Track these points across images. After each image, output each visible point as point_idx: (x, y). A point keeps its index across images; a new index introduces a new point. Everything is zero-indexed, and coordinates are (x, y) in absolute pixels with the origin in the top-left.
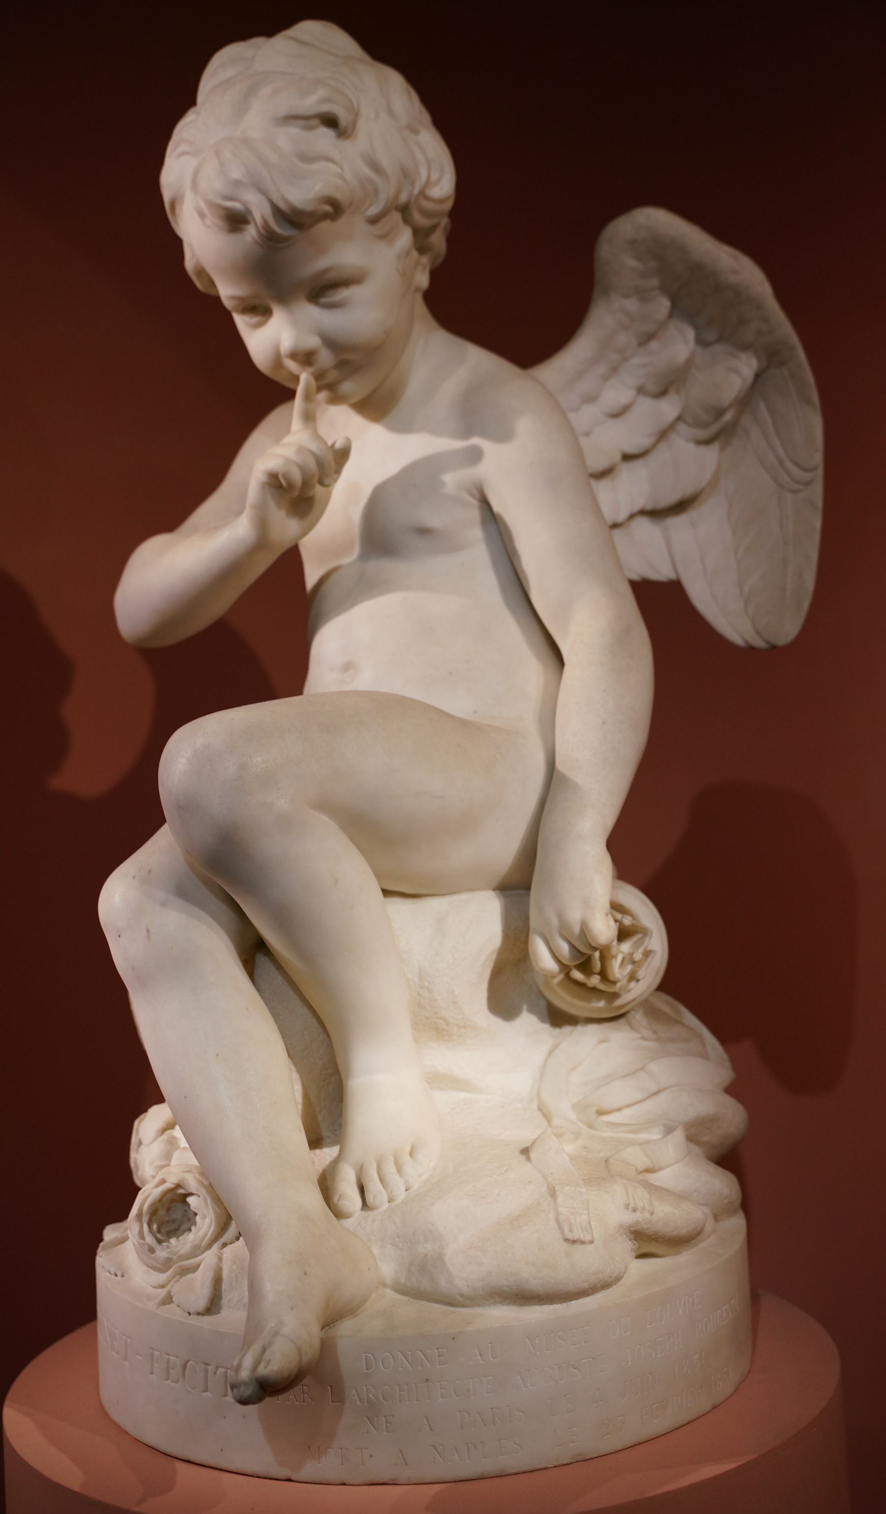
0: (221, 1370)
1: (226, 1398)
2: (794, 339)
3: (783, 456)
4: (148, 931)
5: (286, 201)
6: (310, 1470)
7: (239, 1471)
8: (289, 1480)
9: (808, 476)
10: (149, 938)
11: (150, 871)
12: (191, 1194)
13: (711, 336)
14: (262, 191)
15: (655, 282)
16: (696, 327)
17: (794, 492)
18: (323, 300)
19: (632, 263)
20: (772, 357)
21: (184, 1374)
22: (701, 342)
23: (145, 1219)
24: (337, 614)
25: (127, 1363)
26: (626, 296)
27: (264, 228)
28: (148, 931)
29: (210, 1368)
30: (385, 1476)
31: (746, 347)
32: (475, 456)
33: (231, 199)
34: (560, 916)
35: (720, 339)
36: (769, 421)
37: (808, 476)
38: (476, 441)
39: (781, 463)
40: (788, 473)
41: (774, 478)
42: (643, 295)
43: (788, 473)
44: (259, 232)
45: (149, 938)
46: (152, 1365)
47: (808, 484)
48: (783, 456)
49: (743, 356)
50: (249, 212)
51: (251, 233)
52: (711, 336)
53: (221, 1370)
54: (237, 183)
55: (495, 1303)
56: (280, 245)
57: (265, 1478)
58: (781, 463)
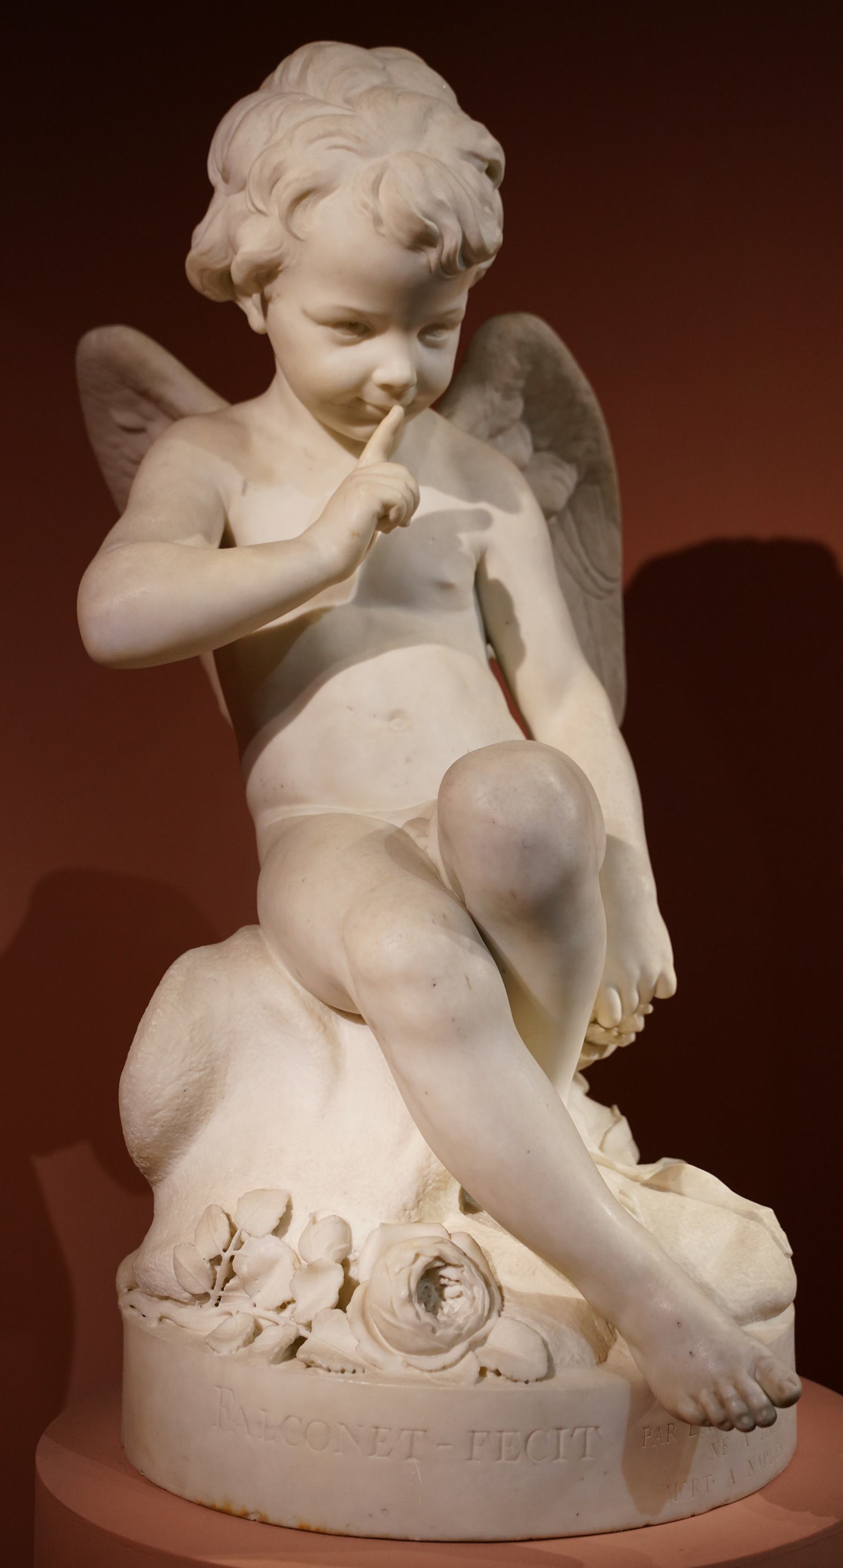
0: (578, 1432)
1: (585, 1459)
2: (612, 463)
3: (587, 563)
4: (467, 979)
5: (480, 237)
6: (669, 1509)
7: (597, 1531)
8: (647, 1526)
9: (611, 585)
10: (470, 987)
11: (444, 916)
12: (447, 1265)
13: (544, 443)
14: (460, 221)
15: (521, 383)
16: (534, 433)
17: (599, 598)
18: (429, 338)
19: (514, 361)
20: (590, 475)
21: (526, 1448)
22: (536, 449)
23: (415, 1298)
24: (363, 659)
25: (413, 1461)
26: (497, 390)
27: (448, 257)
28: (467, 979)
29: (563, 1433)
30: (721, 1500)
31: (570, 460)
32: (484, 521)
33: (430, 219)
34: (644, 970)
35: (550, 448)
36: (574, 529)
37: (611, 585)
38: (483, 506)
39: (586, 570)
40: (593, 580)
41: (580, 583)
42: (507, 393)
43: (593, 580)
44: (439, 259)
45: (470, 987)
46: (472, 1449)
47: (610, 592)
48: (587, 563)
49: (567, 467)
50: (441, 236)
51: (431, 257)
52: (544, 443)
53: (578, 1432)
54: (440, 204)
55: (757, 1320)
56: (448, 277)
57: (624, 1530)
58: (586, 570)
